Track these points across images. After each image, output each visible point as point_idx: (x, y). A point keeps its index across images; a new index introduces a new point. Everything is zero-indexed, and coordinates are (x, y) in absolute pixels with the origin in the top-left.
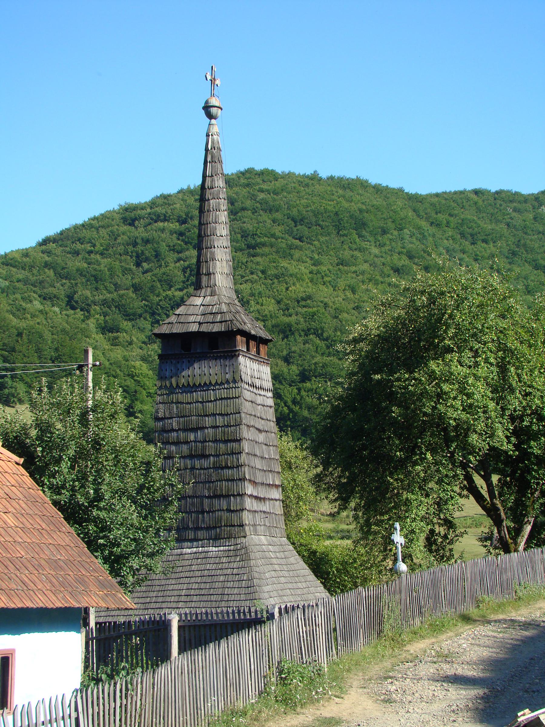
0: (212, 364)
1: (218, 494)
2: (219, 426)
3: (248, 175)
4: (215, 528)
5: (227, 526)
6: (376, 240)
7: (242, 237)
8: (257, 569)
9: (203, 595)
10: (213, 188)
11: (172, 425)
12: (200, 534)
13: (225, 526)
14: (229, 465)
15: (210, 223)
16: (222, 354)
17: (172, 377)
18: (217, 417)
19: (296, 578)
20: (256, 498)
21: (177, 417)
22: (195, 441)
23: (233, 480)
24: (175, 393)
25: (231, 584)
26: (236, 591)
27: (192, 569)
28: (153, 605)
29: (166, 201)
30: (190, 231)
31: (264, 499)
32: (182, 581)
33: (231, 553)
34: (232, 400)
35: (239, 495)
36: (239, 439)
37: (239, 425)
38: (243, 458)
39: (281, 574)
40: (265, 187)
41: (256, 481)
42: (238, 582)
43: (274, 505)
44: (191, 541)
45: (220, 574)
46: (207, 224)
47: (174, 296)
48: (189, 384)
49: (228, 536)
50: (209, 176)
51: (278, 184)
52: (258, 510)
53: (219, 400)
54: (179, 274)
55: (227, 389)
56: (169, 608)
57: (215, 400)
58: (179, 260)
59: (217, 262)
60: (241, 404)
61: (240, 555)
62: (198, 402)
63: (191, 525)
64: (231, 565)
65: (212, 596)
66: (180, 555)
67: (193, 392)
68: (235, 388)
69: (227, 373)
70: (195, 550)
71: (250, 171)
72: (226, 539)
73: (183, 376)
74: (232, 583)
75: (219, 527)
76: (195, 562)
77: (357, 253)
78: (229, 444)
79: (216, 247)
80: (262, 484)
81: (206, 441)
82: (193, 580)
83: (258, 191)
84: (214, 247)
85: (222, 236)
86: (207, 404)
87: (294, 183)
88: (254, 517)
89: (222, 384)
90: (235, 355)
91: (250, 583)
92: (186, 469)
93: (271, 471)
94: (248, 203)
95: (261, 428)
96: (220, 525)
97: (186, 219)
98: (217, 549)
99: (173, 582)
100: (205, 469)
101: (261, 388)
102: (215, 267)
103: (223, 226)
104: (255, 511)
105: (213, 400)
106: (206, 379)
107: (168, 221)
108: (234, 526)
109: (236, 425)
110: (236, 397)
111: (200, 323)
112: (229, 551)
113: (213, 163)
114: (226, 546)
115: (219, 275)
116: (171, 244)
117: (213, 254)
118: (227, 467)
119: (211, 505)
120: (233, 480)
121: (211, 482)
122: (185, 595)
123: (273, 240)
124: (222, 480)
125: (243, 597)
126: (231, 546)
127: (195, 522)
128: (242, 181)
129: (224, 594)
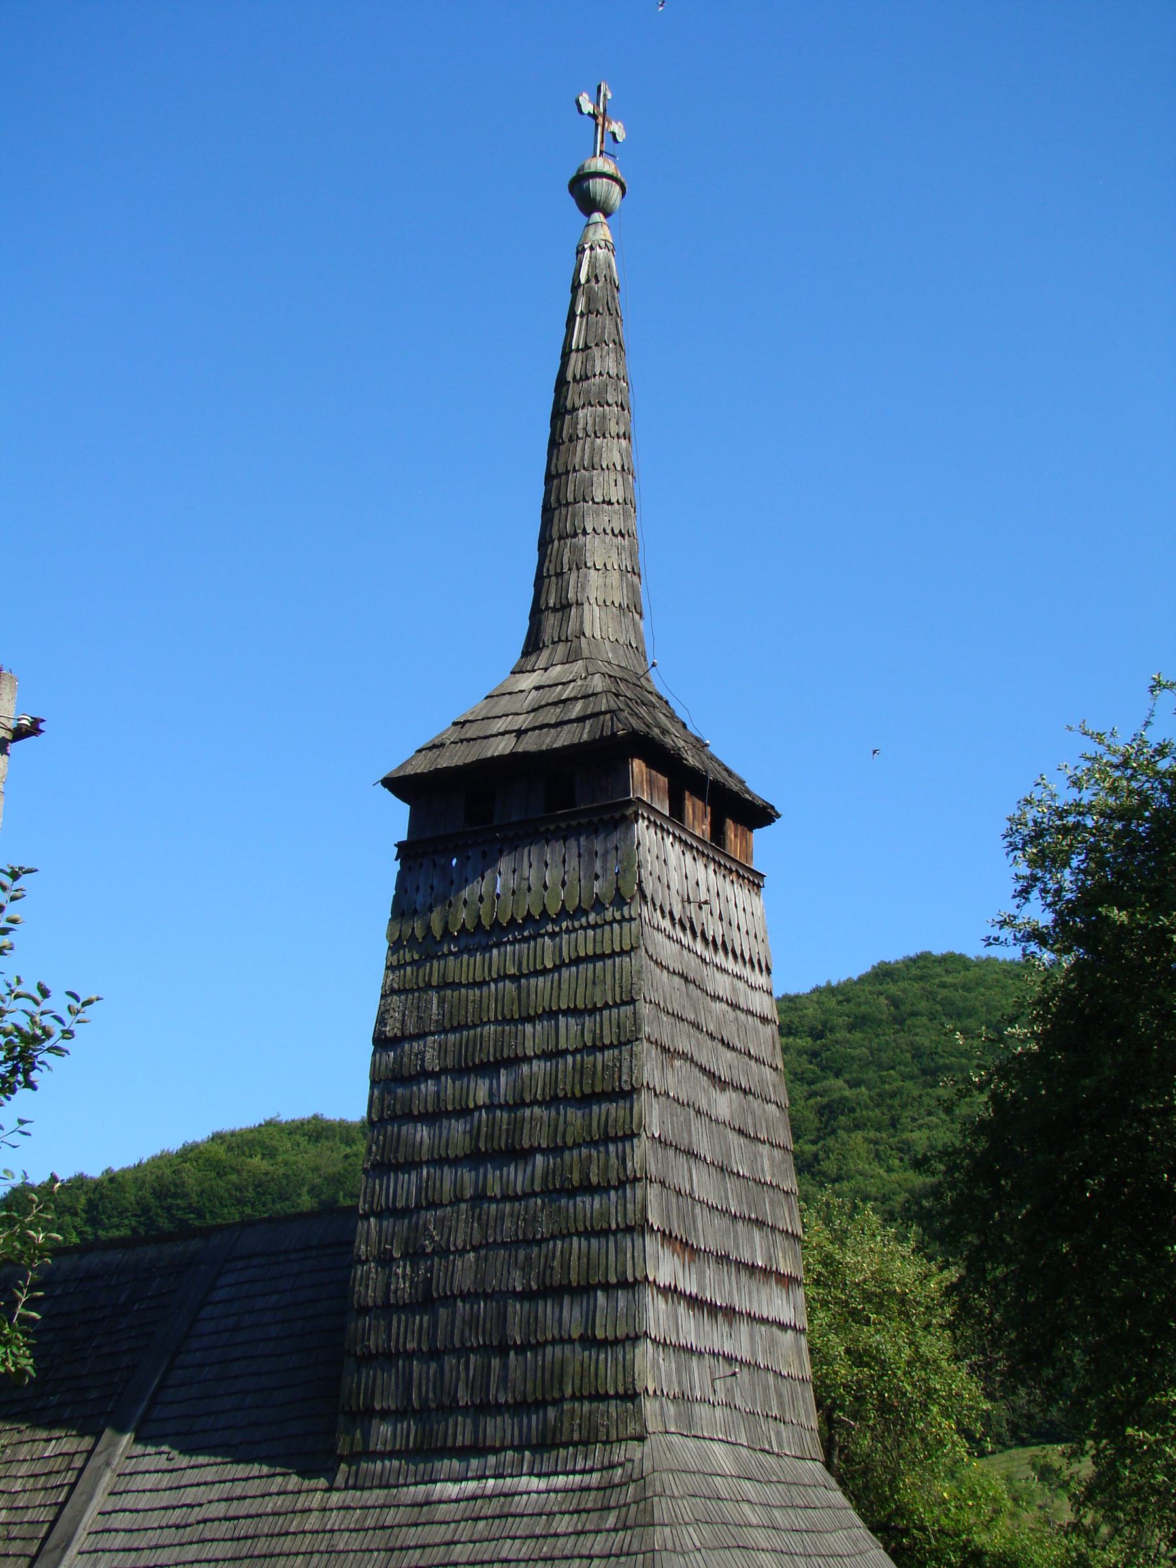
0: (552, 853)
1: (556, 1283)
2: (564, 1053)
3: (921, 963)
4: (541, 1405)
5: (581, 1398)
7: (913, 1057)
10: (587, 378)
11: (423, 1060)
12: (495, 1428)
14: (594, 1180)
15: (575, 471)
16: (584, 821)
17: (431, 910)
18: (562, 1020)
20: (694, 1302)
21: (439, 1033)
22: (490, 1107)
23: (605, 1233)
24: (439, 958)
29: (791, 1005)
30: (828, 1050)
33: (590, 1500)
34: (609, 962)
35: (623, 1284)
36: (627, 1088)
37: (629, 1042)
38: (643, 1155)
40: (948, 979)
41: (692, 1241)
43: (773, 1342)
44: (463, 1453)
46: (567, 472)
47: (802, 1152)
48: (479, 925)
50: (578, 350)
51: (970, 974)
53: (568, 966)
54: (812, 1116)
55: (594, 927)
57: (557, 968)
58: (812, 1095)
59: (592, 571)
60: (639, 972)
61: (618, 1507)
62: (506, 977)
63: (463, 1399)
66: (421, 1505)
67: (489, 948)
68: (619, 922)
69: (597, 877)
70: (471, 1486)
71: (924, 957)
72: (575, 1444)
73: (465, 902)
78: (595, 1108)
79: (589, 530)
80: (723, 1258)
83: (939, 986)
84: (585, 533)
85: (610, 503)
86: (533, 981)
87: (996, 972)
89: (580, 911)
90: (624, 818)
92: (458, 1200)
93: (760, 1223)
94: (923, 1005)
95: (724, 1074)
96: (556, 1395)
97: (822, 1031)
98: (542, 1484)
100: (516, 1198)
101: (724, 947)
102: (582, 586)
103: (613, 477)
104: (690, 1351)
105: (549, 965)
106: (530, 904)
107: (795, 1035)
108: (606, 1397)
109: (621, 1044)
110: (623, 953)
111: (520, 733)
113: (592, 317)
114: (574, 1472)
115: (596, 609)
116: (799, 1070)
117: (579, 551)
119: (531, 1323)
120: (605, 1233)
121: (530, 1242)
123: (964, 1061)
124: (570, 1235)
126: (591, 1471)
127: (477, 1384)
128: (914, 971)
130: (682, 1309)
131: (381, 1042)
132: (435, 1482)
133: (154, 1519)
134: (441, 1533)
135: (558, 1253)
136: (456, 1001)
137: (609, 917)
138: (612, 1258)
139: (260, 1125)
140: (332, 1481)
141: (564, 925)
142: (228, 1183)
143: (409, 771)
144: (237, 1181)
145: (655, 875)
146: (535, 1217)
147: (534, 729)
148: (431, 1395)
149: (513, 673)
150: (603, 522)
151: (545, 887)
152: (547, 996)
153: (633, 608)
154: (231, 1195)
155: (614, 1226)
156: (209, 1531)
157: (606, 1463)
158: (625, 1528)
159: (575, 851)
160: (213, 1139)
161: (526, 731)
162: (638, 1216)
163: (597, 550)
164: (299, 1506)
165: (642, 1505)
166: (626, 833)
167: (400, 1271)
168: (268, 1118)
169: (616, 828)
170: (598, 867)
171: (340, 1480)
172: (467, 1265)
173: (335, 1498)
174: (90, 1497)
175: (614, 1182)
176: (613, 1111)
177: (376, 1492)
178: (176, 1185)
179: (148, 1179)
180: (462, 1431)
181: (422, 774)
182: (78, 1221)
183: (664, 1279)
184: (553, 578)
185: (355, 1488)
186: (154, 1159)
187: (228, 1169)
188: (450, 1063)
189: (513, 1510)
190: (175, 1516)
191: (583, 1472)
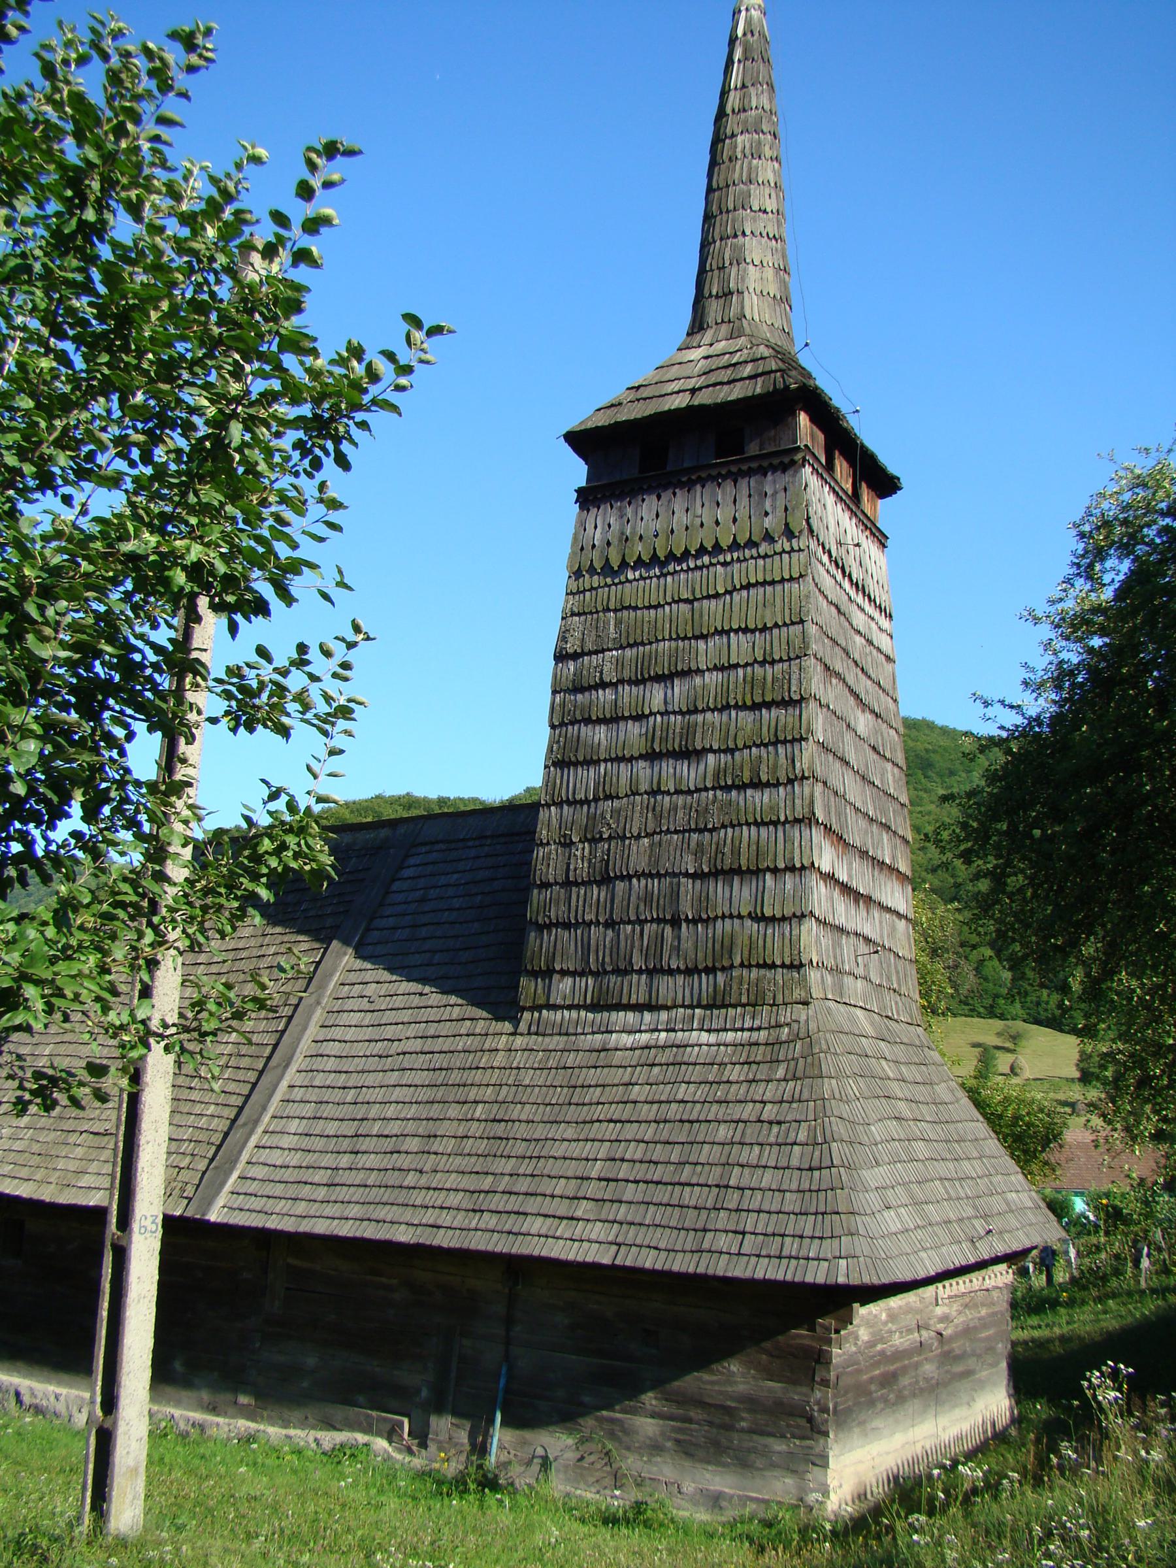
0: (724, 494)
2: (737, 666)
6: (943, 782)
8: (844, 1110)
9: (658, 1183)
11: (601, 673)
12: (668, 988)
13: (742, 965)
14: (764, 778)
19: (956, 1145)
20: (846, 889)
25: (751, 1155)
26: (768, 1179)
27: (632, 1097)
28: (497, 1202)
31: (869, 900)
32: (596, 1130)
33: (759, 1054)
34: (779, 587)
36: (796, 697)
37: (798, 657)
39: (916, 1129)
42: (775, 1149)
43: (893, 929)
45: (720, 1117)
46: (728, 186)
49: (752, 998)
52: (850, 926)
56: (546, 1216)
59: (751, 266)
60: (808, 597)
62: (680, 601)
63: (638, 962)
64: (758, 1091)
65: (688, 1189)
69: (766, 514)
70: (644, 1038)
72: (744, 1006)
74: (756, 1149)
75: (723, 969)
76: (642, 1074)
77: (921, 793)
79: (748, 232)
80: (864, 854)
81: (696, 711)
82: (630, 1131)
84: (744, 234)
85: (765, 212)
88: (837, 945)
90: (793, 463)
91: (817, 1153)
93: (887, 827)
96: (726, 963)
98: (713, 1038)
99: (570, 1132)
100: (689, 792)
103: (767, 191)
104: (841, 930)
108: (773, 966)
110: (791, 579)
111: (693, 391)
112: (751, 1045)
113: (748, 63)
114: (742, 1030)
118: (757, 784)
119: (703, 900)
122: (600, 1179)
125: (791, 1202)
126: (759, 1029)
129: (727, 1187)
130: (836, 893)
131: (561, 657)
132: (611, 1032)
133: (360, 1049)
135: (729, 841)
136: (632, 622)
137: (778, 548)
138: (780, 846)
140: (516, 1027)
141: (735, 555)
143: (590, 425)
146: (706, 810)
147: (708, 386)
148: (607, 959)
149: (680, 349)
150: (760, 227)
151: (717, 523)
152: (719, 617)
153: (784, 300)
155: (782, 819)
156: (407, 1061)
157: (773, 1023)
158: (795, 1078)
159: (745, 492)
161: (700, 389)
162: (806, 810)
163: (755, 249)
164: (486, 1046)
165: (809, 1059)
166: (794, 476)
167: (578, 853)
169: (784, 471)
170: (768, 506)
171: (523, 1027)
172: (642, 849)
173: (519, 1041)
174: (305, 1029)
175: (783, 780)
176: (782, 718)
177: (556, 1038)
180: (637, 988)
181: (603, 427)
183: (826, 867)
184: (716, 272)
185: (536, 1034)
188: (626, 676)
189: (685, 1059)
190: (378, 1048)
191: (751, 1029)
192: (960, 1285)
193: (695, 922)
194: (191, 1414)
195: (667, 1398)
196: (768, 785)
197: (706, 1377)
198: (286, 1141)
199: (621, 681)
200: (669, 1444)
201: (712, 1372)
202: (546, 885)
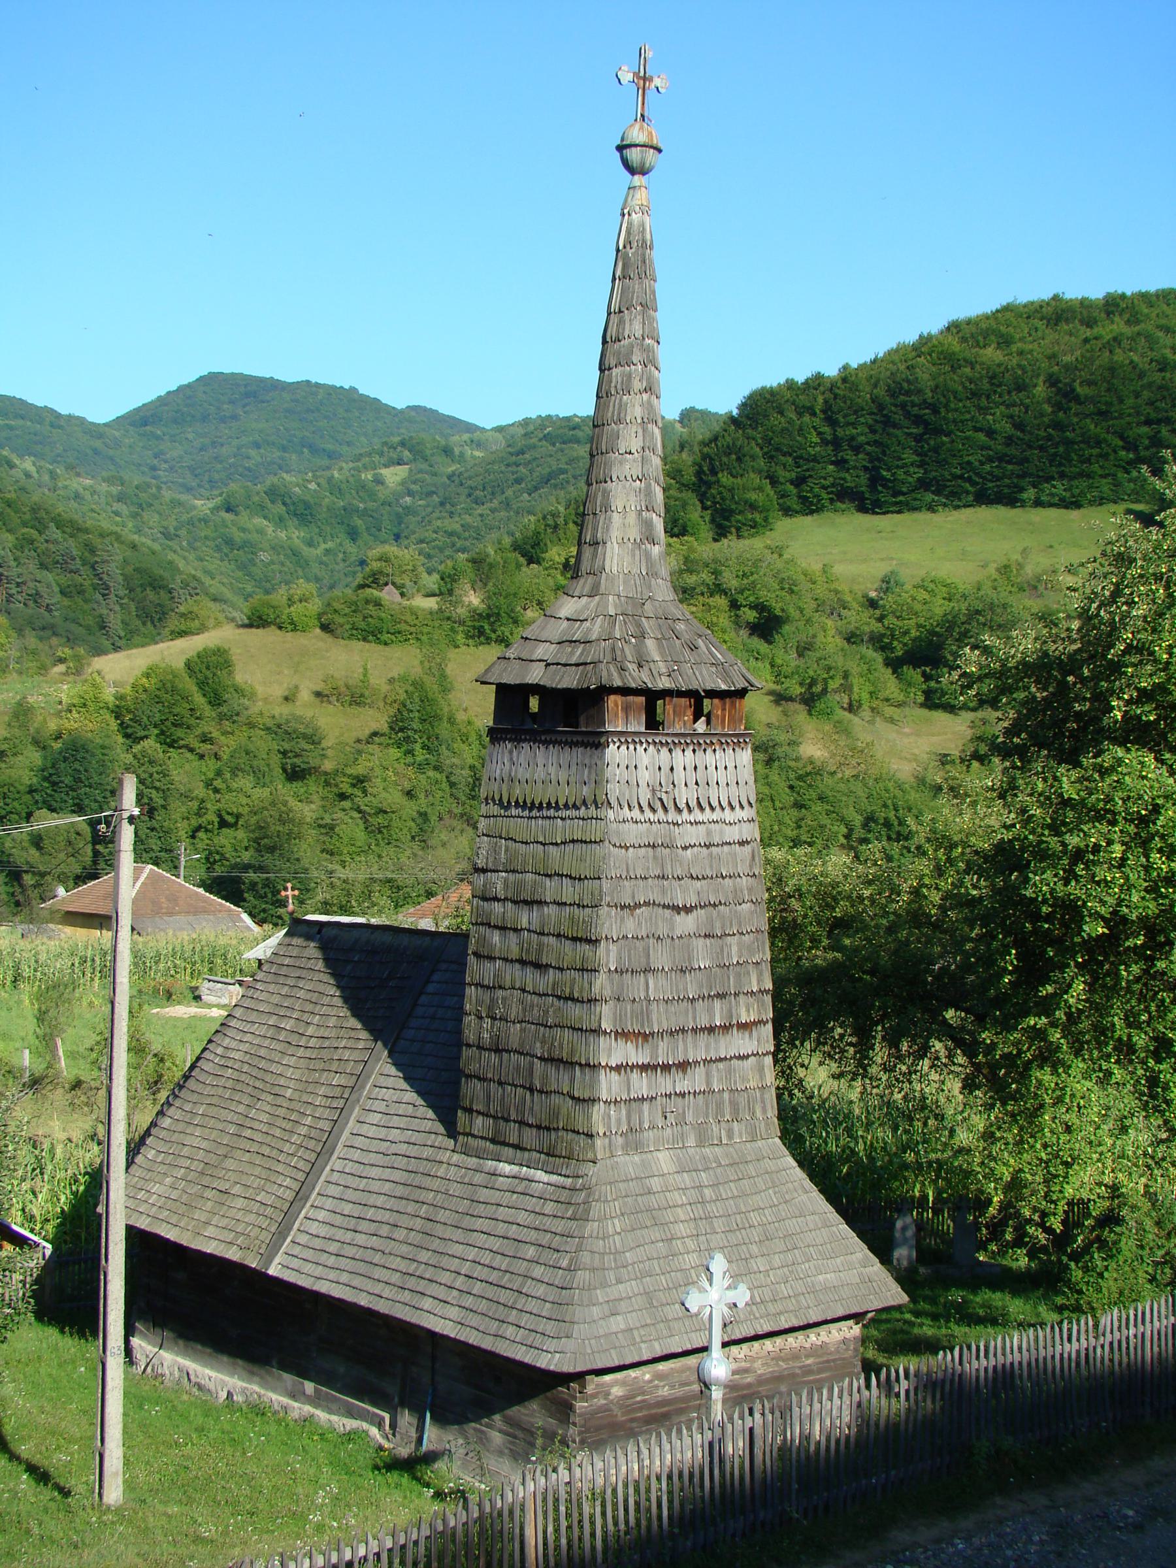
14: (576, 995)
34: (589, 846)
38: (601, 984)
117: (606, 494)
119: (545, 1078)
134: (495, 1196)
139: (997, 311)
142: (961, 377)
144: (970, 375)
145: (623, 781)
154: (965, 388)
160: (948, 329)
168: (1004, 303)
173: (456, 1158)
178: (908, 381)
179: (882, 376)
180: (512, 1132)
182: (817, 421)
186: (889, 353)
187: (962, 362)
192: (768, 1344)
193: (541, 1092)
194: (281, 1398)
195: (508, 1421)
196: (577, 1000)
197: (523, 1410)
198: (322, 1215)
199: (506, 899)
200: (506, 1451)
201: (525, 1407)
202: (469, 1046)
